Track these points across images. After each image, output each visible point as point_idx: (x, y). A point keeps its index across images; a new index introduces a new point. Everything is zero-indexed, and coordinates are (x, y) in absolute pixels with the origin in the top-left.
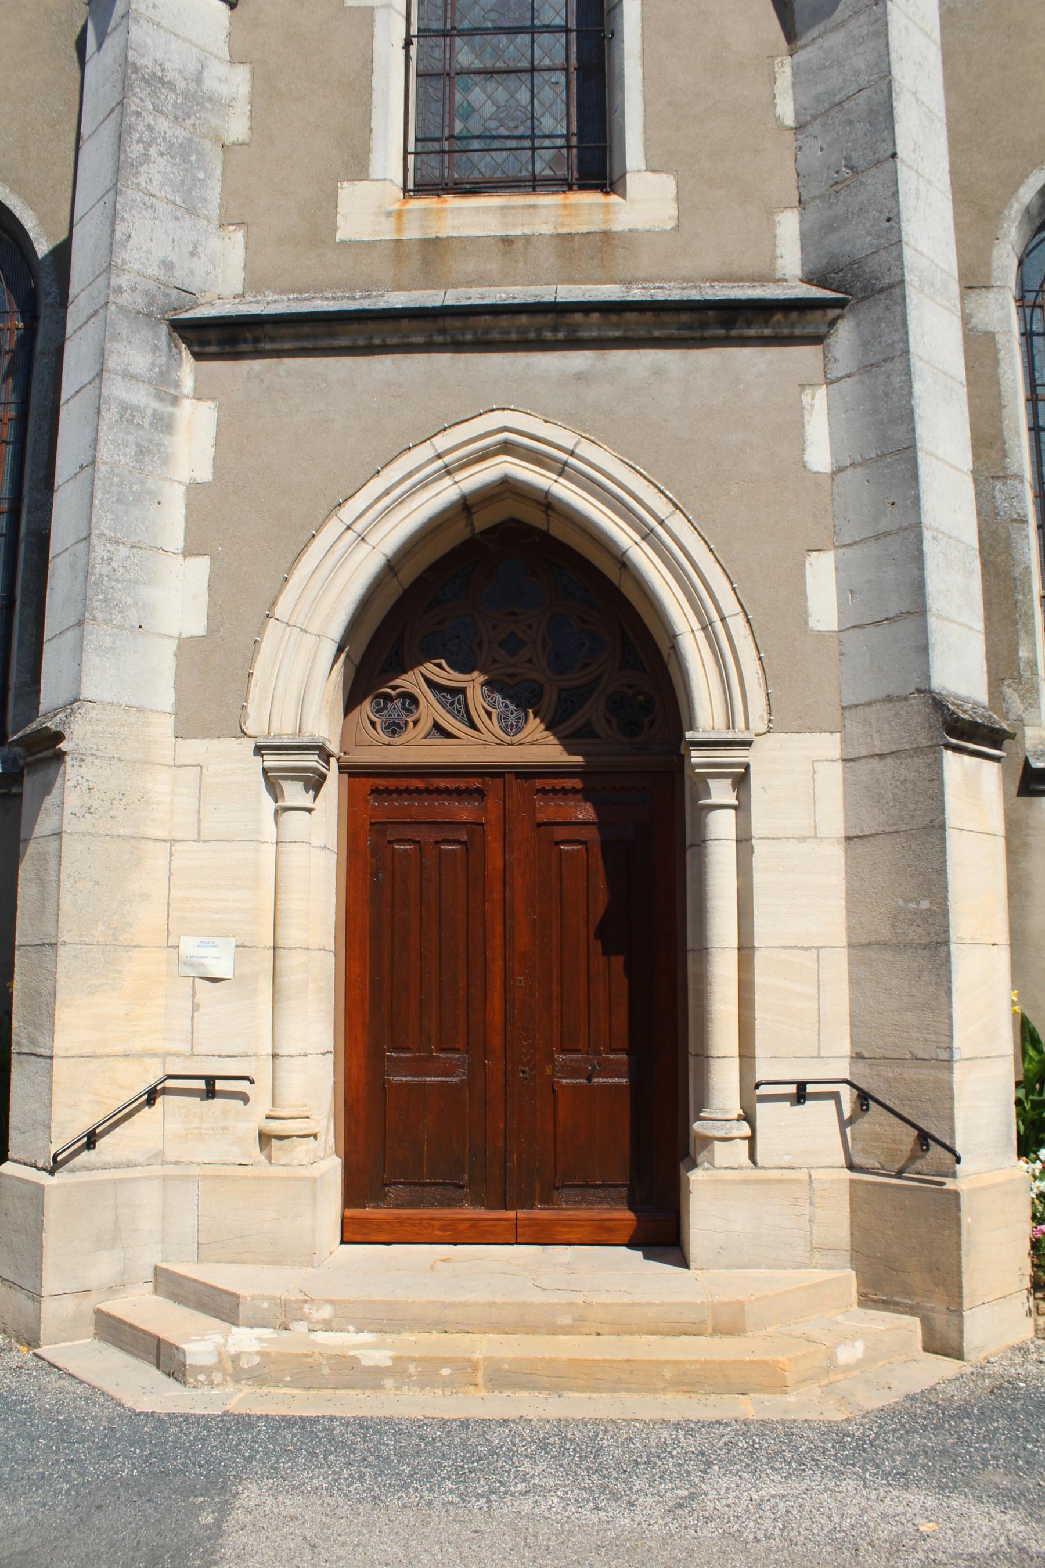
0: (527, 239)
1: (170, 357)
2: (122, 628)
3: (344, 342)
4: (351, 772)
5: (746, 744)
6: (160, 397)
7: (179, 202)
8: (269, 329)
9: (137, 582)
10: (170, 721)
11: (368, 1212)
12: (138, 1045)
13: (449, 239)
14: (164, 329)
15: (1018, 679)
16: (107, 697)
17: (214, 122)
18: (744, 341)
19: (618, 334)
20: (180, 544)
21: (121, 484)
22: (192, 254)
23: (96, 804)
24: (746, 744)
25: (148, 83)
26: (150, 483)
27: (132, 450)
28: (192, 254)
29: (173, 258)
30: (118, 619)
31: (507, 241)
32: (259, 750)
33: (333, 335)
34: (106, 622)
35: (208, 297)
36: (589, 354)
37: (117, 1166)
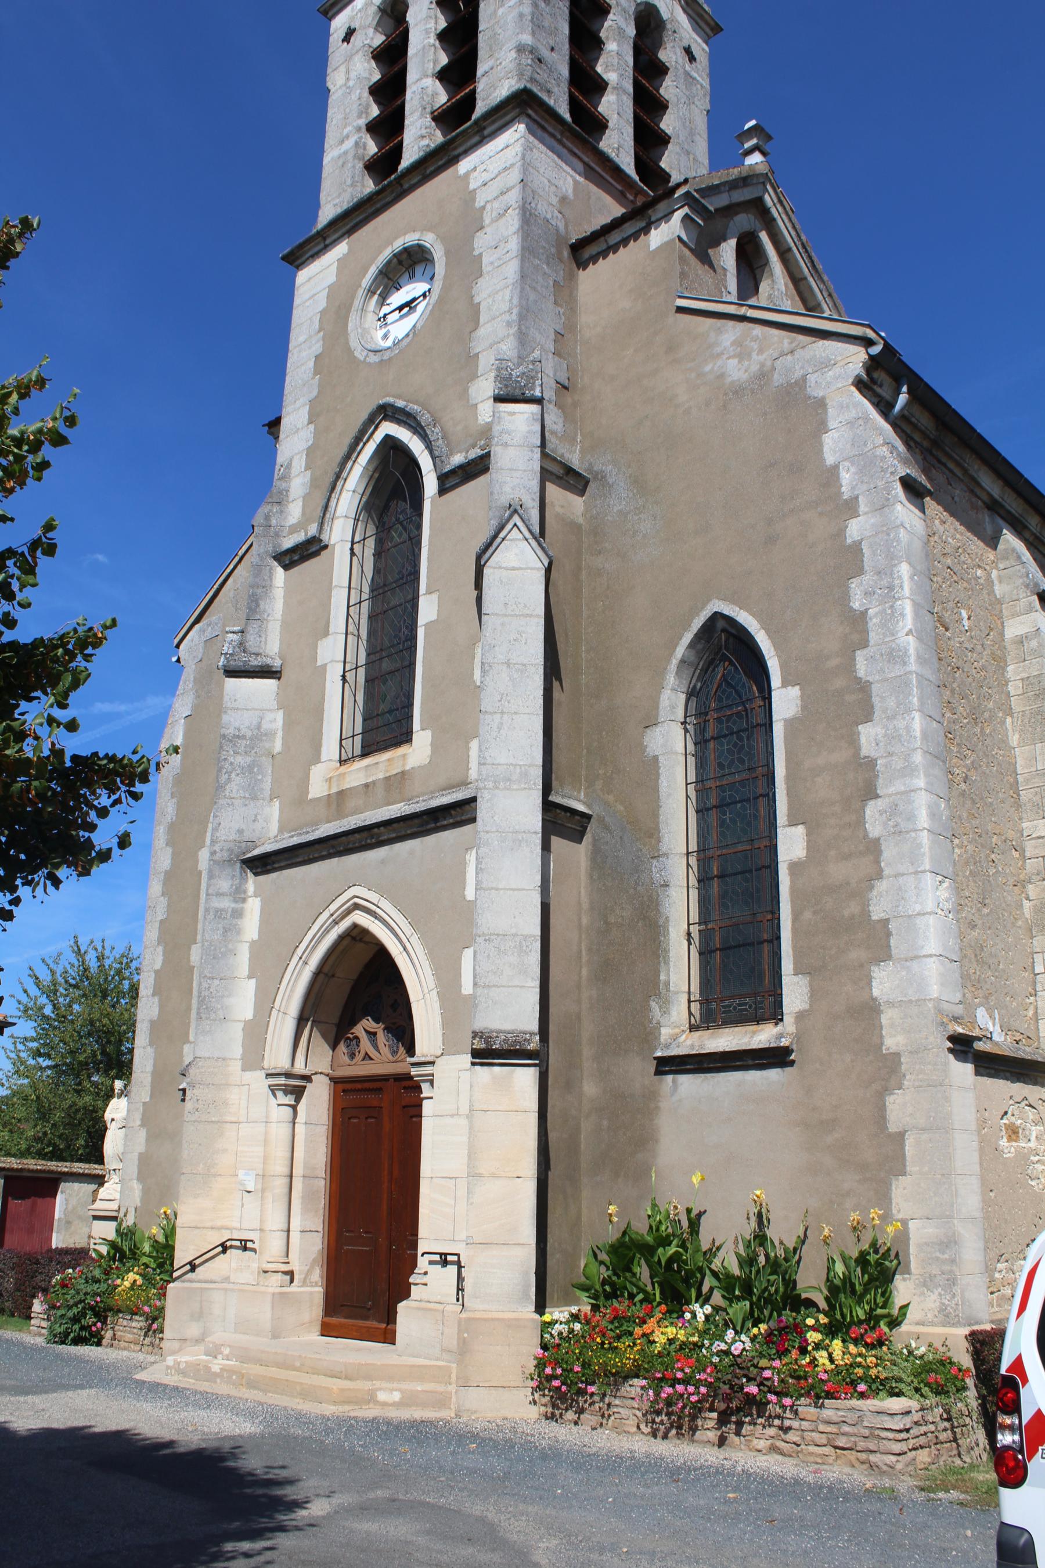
0: (374, 782)
1: (242, 878)
2: (215, 1020)
3: (300, 859)
4: (335, 1081)
5: (433, 1063)
6: (235, 901)
7: (247, 795)
8: (273, 858)
9: (223, 997)
10: (239, 1063)
11: (334, 1320)
12: (219, 1223)
13: (350, 789)
14: (238, 865)
15: (658, 995)
16: (207, 1055)
17: (267, 745)
18: (445, 828)
19: (394, 835)
20: (247, 973)
21: (215, 949)
22: (254, 821)
23: (200, 1107)
24: (433, 1063)
25: (231, 741)
26: (230, 946)
27: (220, 932)
28: (254, 821)
29: (243, 827)
30: (213, 1016)
31: (367, 785)
32: (268, 1075)
33: (297, 856)
34: (207, 1018)
35: (263, 840)
36: (386, 848)
37: (206, 1282)
